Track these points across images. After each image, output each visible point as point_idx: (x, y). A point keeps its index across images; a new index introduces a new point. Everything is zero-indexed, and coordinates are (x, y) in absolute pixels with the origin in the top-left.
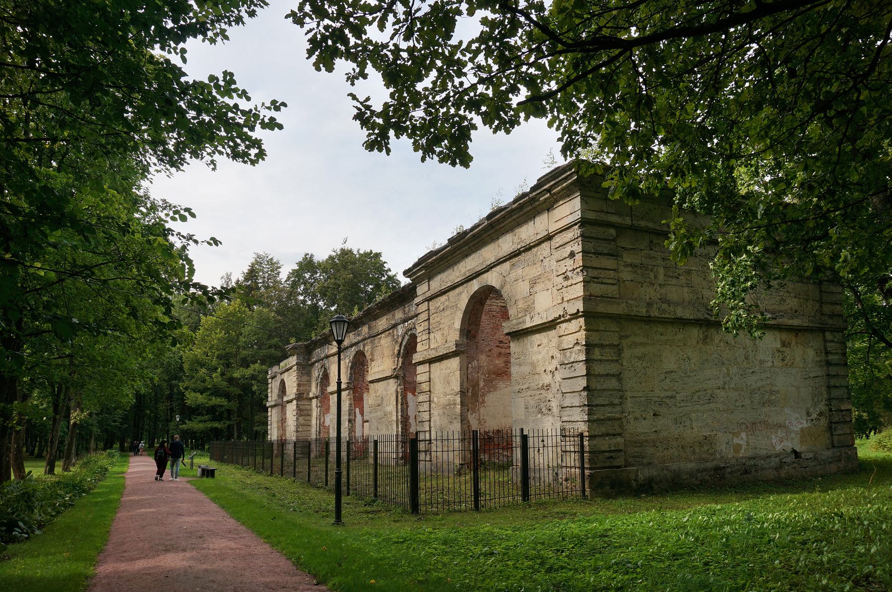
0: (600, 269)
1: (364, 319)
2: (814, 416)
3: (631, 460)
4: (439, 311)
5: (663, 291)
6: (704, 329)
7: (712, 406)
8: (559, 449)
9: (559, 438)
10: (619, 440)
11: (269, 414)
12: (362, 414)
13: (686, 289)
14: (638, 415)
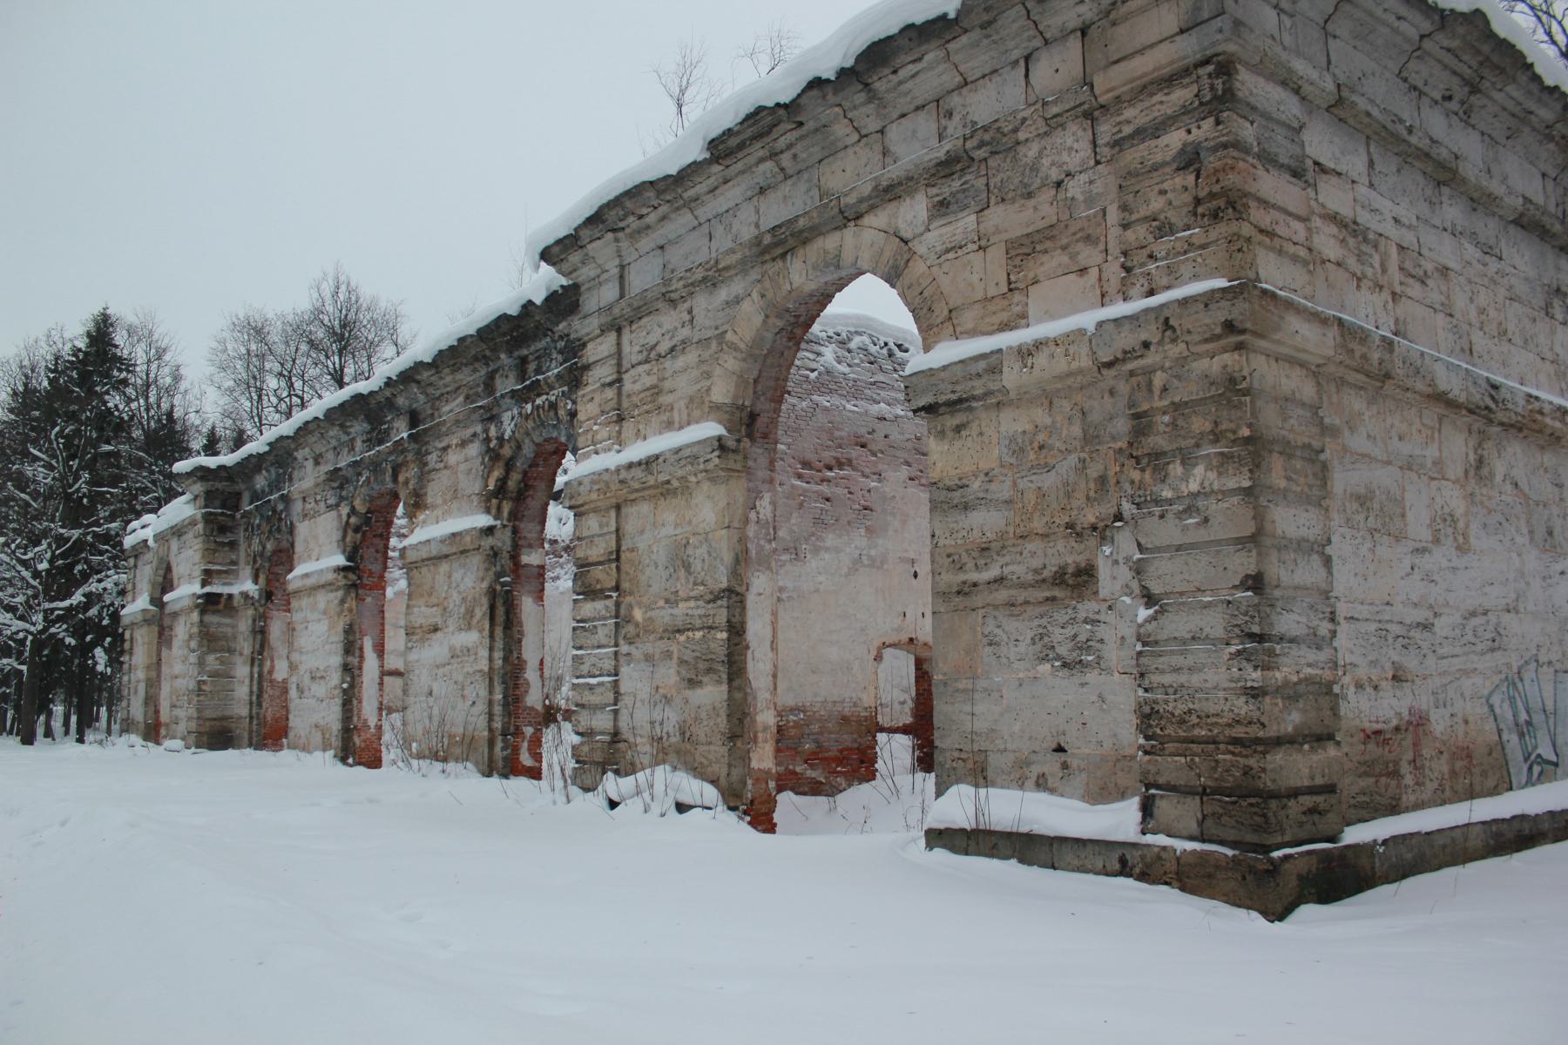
10: (1332, 751)
12: (380, 650)
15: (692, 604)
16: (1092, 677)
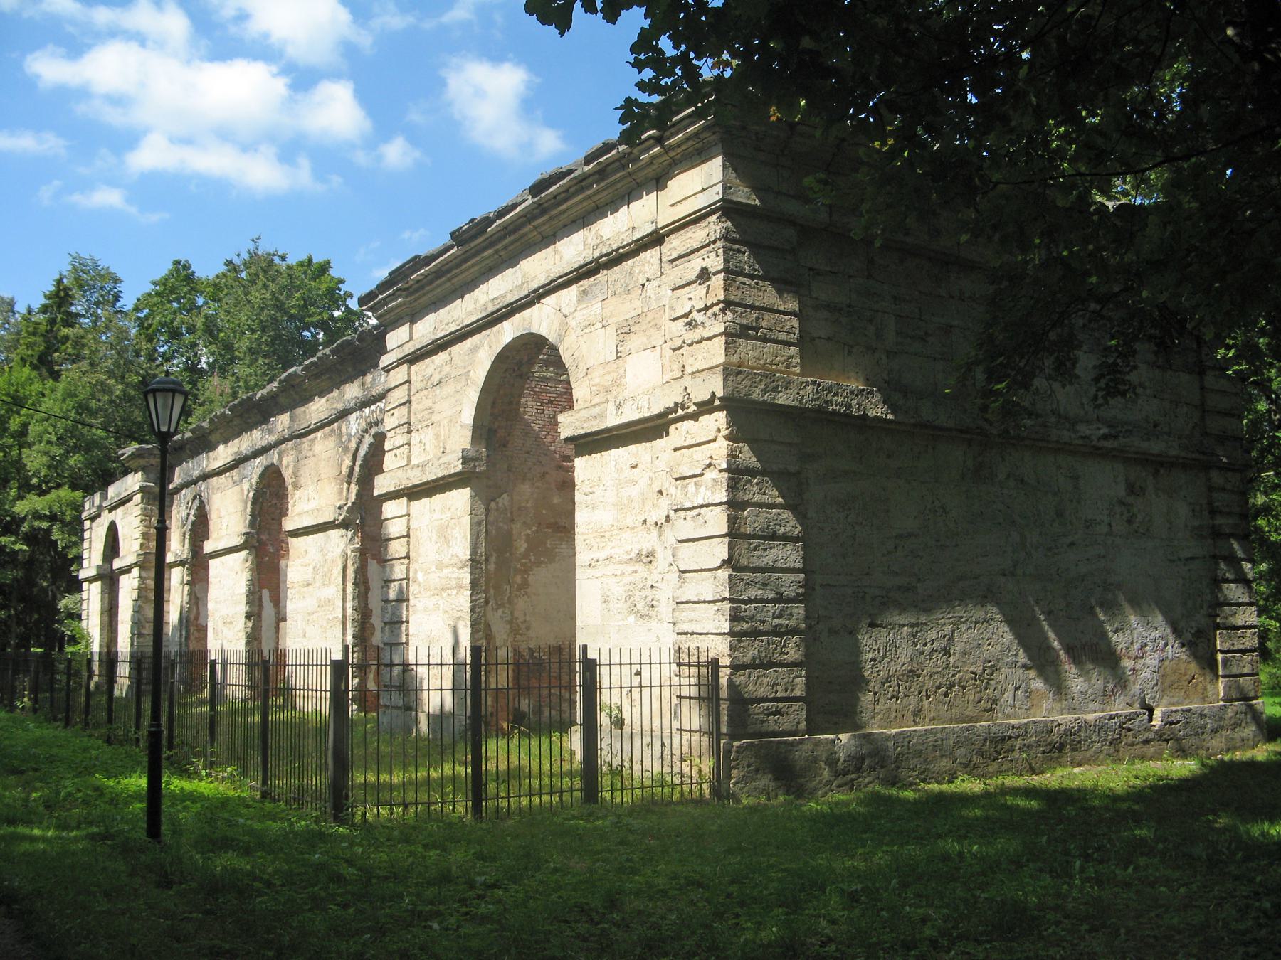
15: (450, 570)
16: (654, 624)
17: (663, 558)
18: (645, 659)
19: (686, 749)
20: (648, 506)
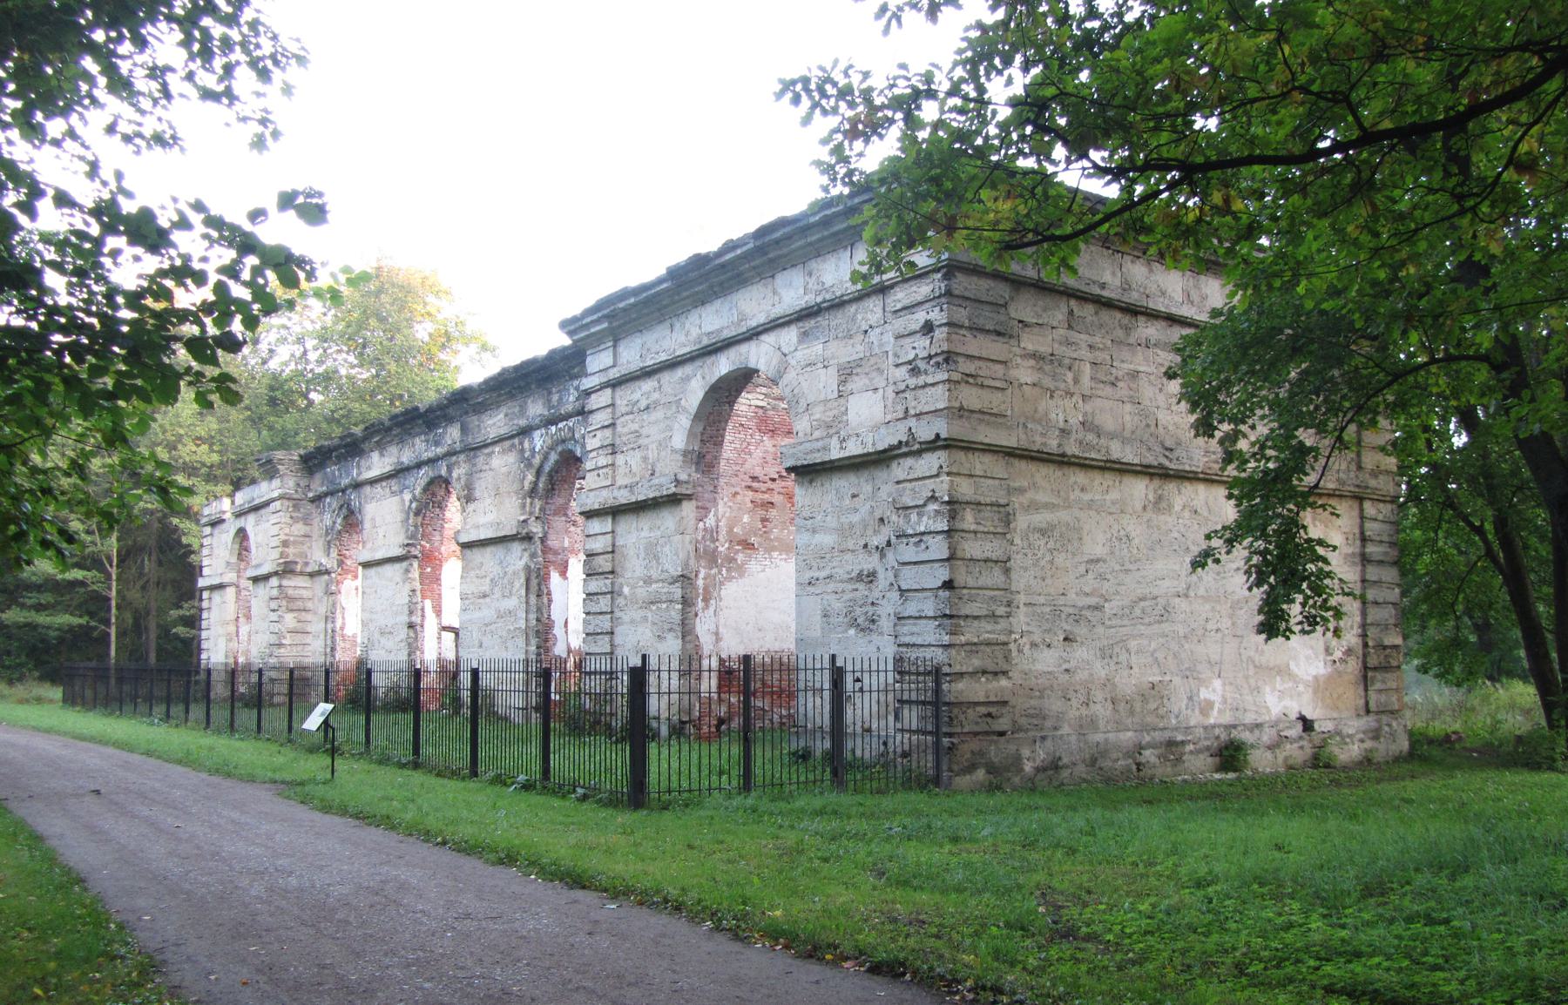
0: (980, 358)
1: (451, 411)
2: (1338, 654)
3: (1023, 721)
4: (634, 410)
5: (1088, 408)
6: (1157, 482)
7: (1166, 627)
8: (891, 696)
9: (890, 675)
10: (1004, 682)
11: (205, 604)
12: (438, 612)
13: (1128, 407)
14: (1037, 638)
16: (874, 637)
17: (884, 578)
18: (866, 667)
19: (906, 747)
20: (870, 532)
